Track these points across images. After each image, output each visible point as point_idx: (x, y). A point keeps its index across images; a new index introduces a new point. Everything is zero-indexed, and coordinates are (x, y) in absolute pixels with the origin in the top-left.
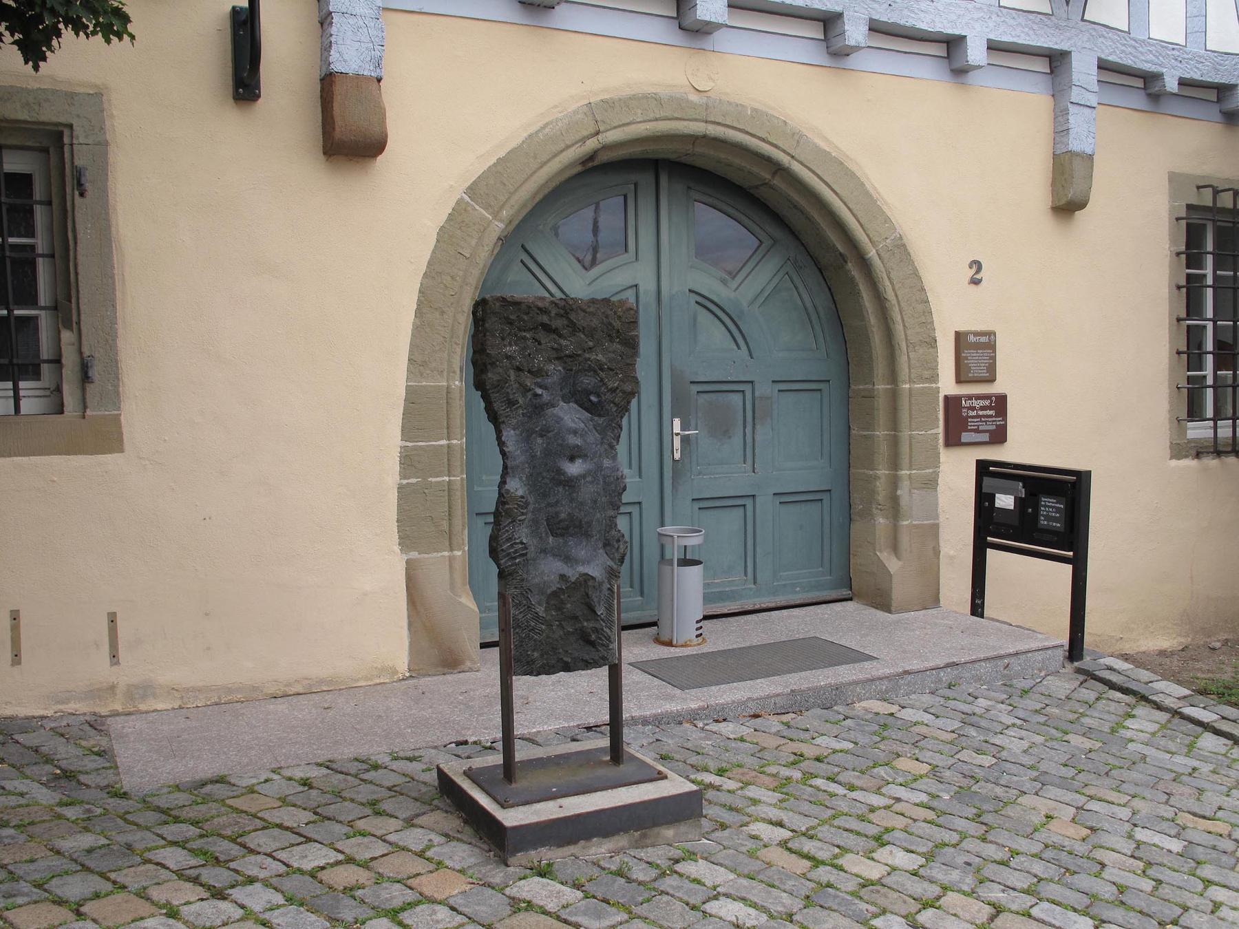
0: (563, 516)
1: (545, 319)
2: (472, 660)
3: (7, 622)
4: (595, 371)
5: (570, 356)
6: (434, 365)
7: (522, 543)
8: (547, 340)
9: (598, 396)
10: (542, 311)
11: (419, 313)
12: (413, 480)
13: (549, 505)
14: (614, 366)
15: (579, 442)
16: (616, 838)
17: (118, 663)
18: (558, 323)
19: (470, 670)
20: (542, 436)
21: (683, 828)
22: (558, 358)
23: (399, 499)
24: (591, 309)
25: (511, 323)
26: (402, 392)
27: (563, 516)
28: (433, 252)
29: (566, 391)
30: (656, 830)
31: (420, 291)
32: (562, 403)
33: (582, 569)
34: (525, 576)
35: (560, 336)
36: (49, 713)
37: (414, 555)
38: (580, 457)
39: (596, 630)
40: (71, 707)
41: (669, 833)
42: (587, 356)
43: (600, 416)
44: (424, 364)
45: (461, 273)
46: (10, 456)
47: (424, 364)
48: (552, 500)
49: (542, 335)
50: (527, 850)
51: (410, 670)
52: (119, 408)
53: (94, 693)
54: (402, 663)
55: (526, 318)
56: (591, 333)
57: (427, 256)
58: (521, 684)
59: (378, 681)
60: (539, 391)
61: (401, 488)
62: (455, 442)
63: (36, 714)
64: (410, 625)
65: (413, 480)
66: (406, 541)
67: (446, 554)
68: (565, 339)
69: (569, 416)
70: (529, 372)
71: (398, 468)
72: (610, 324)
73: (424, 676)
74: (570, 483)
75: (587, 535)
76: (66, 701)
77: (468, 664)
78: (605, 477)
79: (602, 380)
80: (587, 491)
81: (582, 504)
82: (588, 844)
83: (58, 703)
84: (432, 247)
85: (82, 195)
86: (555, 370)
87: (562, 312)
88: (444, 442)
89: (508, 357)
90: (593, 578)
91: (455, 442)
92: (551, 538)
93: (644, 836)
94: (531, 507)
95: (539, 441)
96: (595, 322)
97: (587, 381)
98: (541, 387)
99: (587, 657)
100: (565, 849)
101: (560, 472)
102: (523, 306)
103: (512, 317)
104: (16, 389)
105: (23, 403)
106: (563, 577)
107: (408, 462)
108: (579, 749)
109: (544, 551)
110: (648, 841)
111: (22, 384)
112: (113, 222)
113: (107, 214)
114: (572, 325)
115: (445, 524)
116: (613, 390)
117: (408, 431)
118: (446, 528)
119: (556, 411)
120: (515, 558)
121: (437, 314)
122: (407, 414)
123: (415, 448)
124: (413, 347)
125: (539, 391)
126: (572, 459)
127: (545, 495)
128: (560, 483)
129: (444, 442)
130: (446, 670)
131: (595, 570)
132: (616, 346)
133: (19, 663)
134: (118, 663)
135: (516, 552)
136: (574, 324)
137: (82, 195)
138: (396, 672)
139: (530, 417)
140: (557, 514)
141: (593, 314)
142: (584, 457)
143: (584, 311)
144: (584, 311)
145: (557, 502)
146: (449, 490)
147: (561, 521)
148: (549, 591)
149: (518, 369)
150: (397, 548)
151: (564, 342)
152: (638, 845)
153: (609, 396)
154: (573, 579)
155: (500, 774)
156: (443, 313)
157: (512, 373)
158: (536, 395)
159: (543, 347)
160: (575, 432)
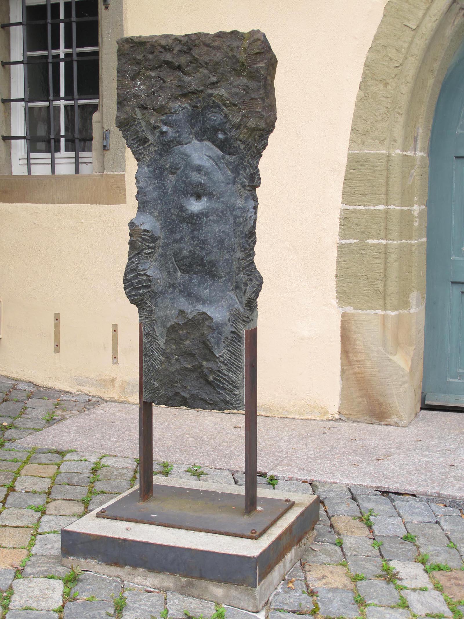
0: (185, 253)
1: (168, 57)
2: (398, 415)
3: (53, 321)
4: (219, 107)
5: (193, 93)
6: (376, 133)
7: (146, 275)
8: (171, 79)
9: (225, 134)
10: (167, 49)
11: (363, 86)
12: (351, 241)
13: (175, 241)
14: (235, 100)
15: (202, 179)
16: (161, 576)
17: (117, 363)
18: (183, 60)
19: (396, 425)
20: (173, 173)
21: (235, 592)
22: (184, 95)
23: (339, 256)
24: (216, 44)
25: (138, 63)
26: (344, 160)
27: (185, 253)
28: (380, 27)
29: (197, 128)
30: (204, 583)
31: (366, 65)
32: (195, 142)
33: (200, 307)
34: (153, 307)
35: (184, 73)
36: (73, 390)
37: (349, 309)
38: (205, 194)
39: (211, 371)
40: (87, 389)
41: (218, 591)
42: (210, 91)
43: (230, 154)
44: (366, 133)
45: (406, 45)
46: (58, 203)
47: (366, 133)
48: (178, 236)
49: (165, 73)
50: (78, 557)
51: (340, 413)
52: (124, 170)
53: (101, 383)
54: (333, 406)
55: (151, 57)
56: (214, 67)
57: (373, 31)
58: (159, 411)
59: (309, 417)
60: (165, 129)
61: (340, 247)
62: (392, 207)
63: (66, 390)
64: (343, 372)
65: (351, 241)
66: (344, 295)
67: (379, 312)
68: (189, 75)
69: (200, 153)
70: (154, 110)
71: (337, 229)
72: (234, 57)
73: (353, 421)
74: (194, 220)
75: (214, 276)
76: (84, 384)
77: (395, 419)
78: (236, 217)
79: (226, 116)
80: (213, 230)
81: (203, 242)
82: (134, 571)
83: (80, 384)
84: (379, 22)
85: (107, 8)
86: (181, 107)
87: (185, 48)
88: (382, 207)
89: (136, 96)
90: (211, 318)
91: (392, 207)
92: (179, 274)
93: (190, 585)
94: (161, 242)
95: (172, 178)
96: (218, 56)
97: (215, 118)
98: (165, 124)
99: (205, 397)
100: (112, 568)
101: (182, 209)
102: (148, 46)
103: (138, 57)
104: (77, 158)
105: (82, 167)
106: (182, 312)
107: (347, 223)
108: (164, 484)
109: (172, 286)
110: (196, 592)
111: (81, 154)
112: (125, 27)
113: (122, 21)
114: (195, 60)
115: (380, 286)
116: (238, 127)
117: (349, 196)
118: (381, 288)
119: (187, 149)
120: (139, 289)
121: (381, 86)
122: (347, 180)
123: (354, 212)
124: (357, 117)
125: (165, 129)
126: (198, 197)
127: (172, 232)
128: (183, 220)
129: (382, 207)
130: (373, 420)
131: (218, 313)
132: (243, 80)
133: (59, 352)
134: (117, 363)
135: (139, 282)
136: (196, 59)
137: (107, 8)
138: (326, 412)
139: (160, 155)
140: (181, 249)
141: (218, 48)
142: (210, 195)
143: (208, 45)
144: (208, 45)
145: (182, 238)
146: (386, 253)
147: (184, 257)
148: (168, 326)
149: (143, 107)
150: (334, 302)
151: (186, 79)
152: (183, 591)
153: (233, 133)
154: (190, 317)
155: (242, 503)
156: (386, 84)
157: (137, 110)
158: (162, 133)
159: (168, 84)
160: (199, 169)
